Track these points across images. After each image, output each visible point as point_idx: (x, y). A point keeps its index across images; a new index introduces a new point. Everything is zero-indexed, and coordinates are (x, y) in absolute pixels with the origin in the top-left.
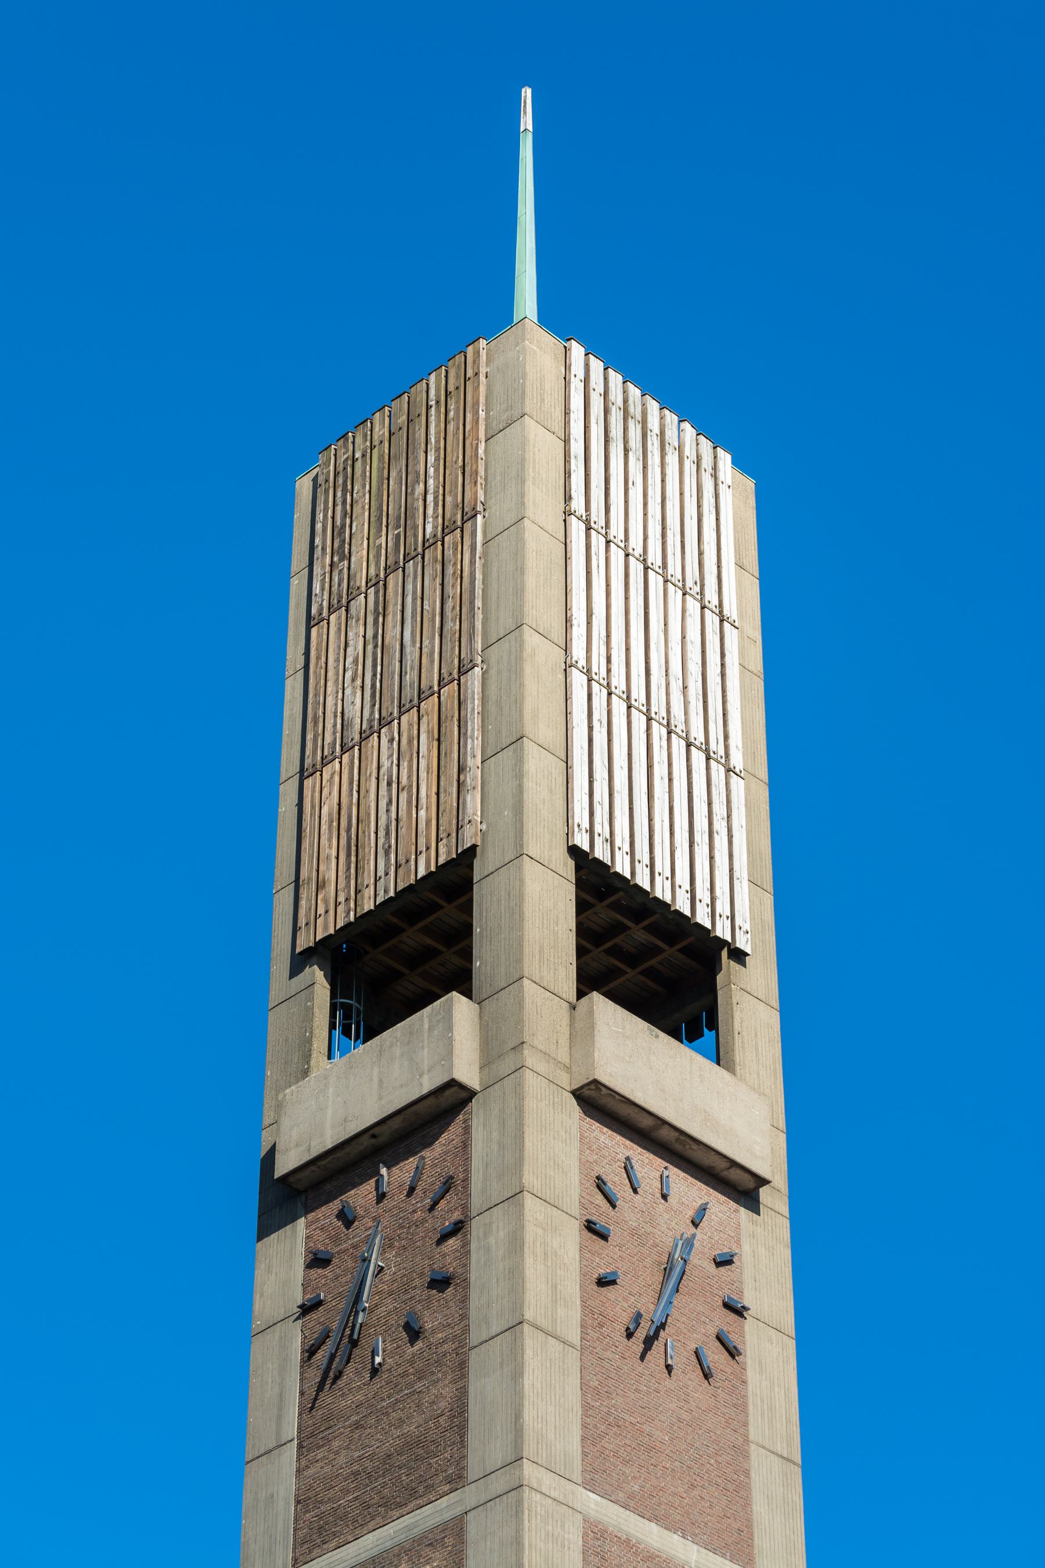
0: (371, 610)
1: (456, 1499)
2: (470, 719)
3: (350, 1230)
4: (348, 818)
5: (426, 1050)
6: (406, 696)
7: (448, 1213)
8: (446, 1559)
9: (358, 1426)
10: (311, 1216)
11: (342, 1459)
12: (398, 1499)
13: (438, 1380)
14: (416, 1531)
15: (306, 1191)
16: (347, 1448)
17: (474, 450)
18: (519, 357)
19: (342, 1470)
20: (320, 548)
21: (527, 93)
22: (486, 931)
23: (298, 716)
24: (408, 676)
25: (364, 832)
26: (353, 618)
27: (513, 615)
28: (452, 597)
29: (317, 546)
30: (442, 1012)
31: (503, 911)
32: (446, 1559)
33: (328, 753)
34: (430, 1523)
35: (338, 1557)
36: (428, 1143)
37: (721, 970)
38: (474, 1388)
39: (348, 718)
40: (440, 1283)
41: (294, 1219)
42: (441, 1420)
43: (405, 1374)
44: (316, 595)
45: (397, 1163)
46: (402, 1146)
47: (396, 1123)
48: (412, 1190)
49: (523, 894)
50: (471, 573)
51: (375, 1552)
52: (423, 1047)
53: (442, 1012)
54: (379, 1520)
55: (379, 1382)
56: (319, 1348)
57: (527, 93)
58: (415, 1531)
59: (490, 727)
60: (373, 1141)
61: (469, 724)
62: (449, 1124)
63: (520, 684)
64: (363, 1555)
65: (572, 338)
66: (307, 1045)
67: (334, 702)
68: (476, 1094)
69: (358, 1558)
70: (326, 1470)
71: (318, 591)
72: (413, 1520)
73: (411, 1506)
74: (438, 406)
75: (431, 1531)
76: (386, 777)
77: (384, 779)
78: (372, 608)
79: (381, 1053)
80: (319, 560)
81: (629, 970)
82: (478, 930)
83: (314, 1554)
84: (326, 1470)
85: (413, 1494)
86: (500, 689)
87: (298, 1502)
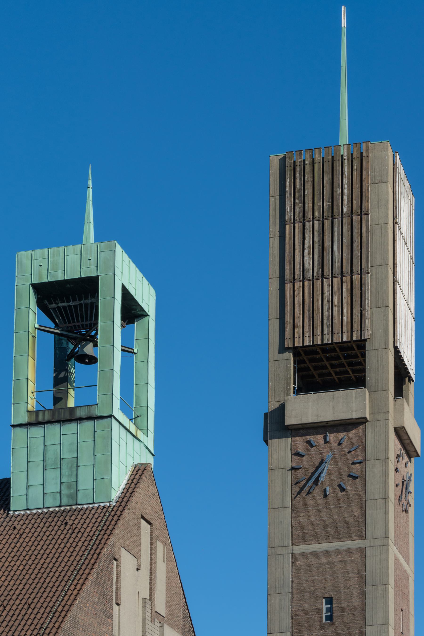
0: (316, 230)
1: (361, 542)
2: (367, 292)
3: (312, 448)
4: (309, 306)
5: (354, 404)
6: (336, 271)
7: (357, 457)
8: (357, 558)
9: (318, 510)
10: (294, 439)
11: (312, 518)
12: (337, 537)
13: (353, 506)
14: (344, 547)
15: (291, 430)
16: (314, 516)
17: (367, 187)
18: (385, 157)
19: (312, 522)
20: (289, 193)
21: (344, 9)
22: (372, 369)
23: (277, 255)
24: (336, 264)
25: (317, 315)
26: (307, 229)
27: (383, 259)
28: (357, 242)
29: (287, 192)
30: (361, 393)
31: (379, 365)
32: (357, 558)
33: (297, 278)
34: (350, 547)
35: (312, 547)
36: (348, 431)
37: (405, 384)
38: (368, 513)
39: (307, 268)
40: (297, 454)
41: (286, 437)
42: (355, 518)
43: (338, 500)
44: (287, 212)
45: (333, 433)
46: (335, 428)
47: (338, 422)
48: (340, 444)
49: (388, 362)
50: (366, 237)
51: (327, 549)
52: (353, 402)
53: (361, 393)
54: (328, 540)
55: (326, 500)
56: (300, 482)
57: (344, 9)
58: (344, 547)
59: (373, 297)
60: (326, 424)
61: (367, 294)
62: (356, 428)
63: (387, 287)
64: (322, 549)
65: (398, 152)
66: (288, 380)
67: (299, 259)
68: (368, 421)
69: (320, 549)
70: (305, 520)
71: (288, 211)
72: (343, 544)
73: (342, 540)
74: (348, 161)
75: (351, 549)
76: (327, 298)
77: (326, 299)
78: (317, 229)
79: (333, 398)
80: (289, 198)
81: (343, 359)
82: (368, 367)
83: (301, 543)
84: (305, 520)
85: (343, 537)
86: (378, 285)
87: (292, 527)
